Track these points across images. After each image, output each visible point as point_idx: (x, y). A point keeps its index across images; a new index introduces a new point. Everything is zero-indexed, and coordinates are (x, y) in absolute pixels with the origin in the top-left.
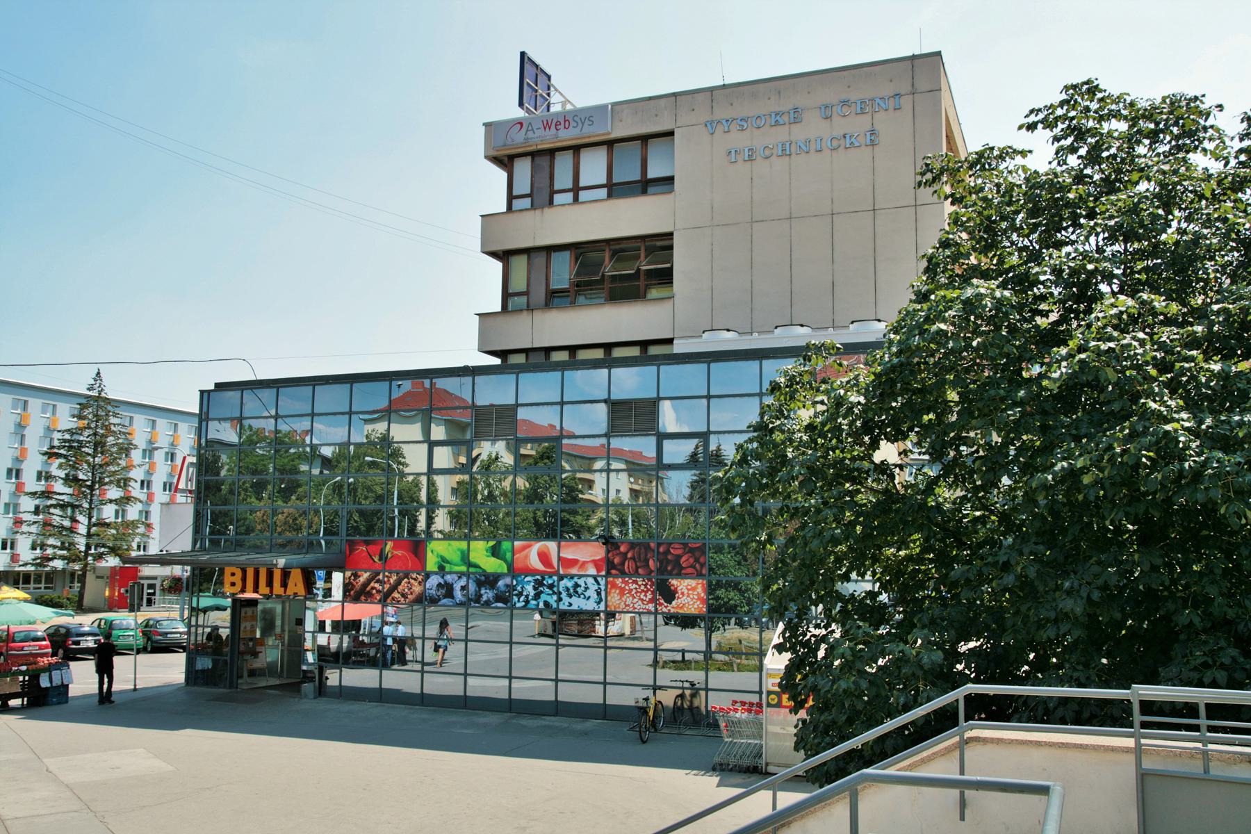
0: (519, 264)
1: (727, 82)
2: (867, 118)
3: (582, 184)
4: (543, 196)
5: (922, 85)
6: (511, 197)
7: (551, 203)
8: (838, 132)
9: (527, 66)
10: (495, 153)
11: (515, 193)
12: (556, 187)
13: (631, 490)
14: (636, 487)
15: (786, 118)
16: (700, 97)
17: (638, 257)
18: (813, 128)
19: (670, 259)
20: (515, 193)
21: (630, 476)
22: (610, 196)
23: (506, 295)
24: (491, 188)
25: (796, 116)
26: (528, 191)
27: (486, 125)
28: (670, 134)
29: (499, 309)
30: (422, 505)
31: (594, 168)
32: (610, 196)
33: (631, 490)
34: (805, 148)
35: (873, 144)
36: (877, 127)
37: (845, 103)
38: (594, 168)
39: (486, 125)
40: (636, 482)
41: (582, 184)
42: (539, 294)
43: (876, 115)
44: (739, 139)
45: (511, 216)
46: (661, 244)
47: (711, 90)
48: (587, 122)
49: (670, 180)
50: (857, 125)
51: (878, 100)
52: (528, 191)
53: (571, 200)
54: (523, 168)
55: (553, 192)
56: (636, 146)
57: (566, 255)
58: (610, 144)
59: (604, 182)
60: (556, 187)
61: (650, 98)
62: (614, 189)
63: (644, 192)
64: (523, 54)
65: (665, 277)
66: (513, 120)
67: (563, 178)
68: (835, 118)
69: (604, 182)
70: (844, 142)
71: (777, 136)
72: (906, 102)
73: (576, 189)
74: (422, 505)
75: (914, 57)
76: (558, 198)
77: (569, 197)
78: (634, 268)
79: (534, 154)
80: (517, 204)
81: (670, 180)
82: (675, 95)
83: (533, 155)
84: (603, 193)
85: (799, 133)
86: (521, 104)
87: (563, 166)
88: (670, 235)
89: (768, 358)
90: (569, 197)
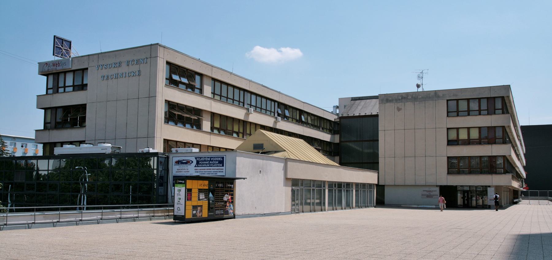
0: (49, 112)
3: (66, 85)
5: (153, 55)
6: (47, 89)
7: (58, 92)
8: (130, 71)
9: (56, 40)
16: (95, 56)
18: (124, 69)
22: (74, 90)
23: (45, 123)
24: (41, 84)
27: (38, 63)
28: (87, 69)
29: (43, 128)
30: (35, 170)
31: (69, 81)
32: (74, 90)
35: (139, 75)
37: (133, 61)
39: (38, 63)
41: (66, 85)
43: (142, 65)
44: (105, 72)
46: (83, 107)
47: (98, 54)
50: (135, 68)
52: (486, 109)
54: (51, 78)
55: (495, 109)
57: (61, 109)
58: (74, 71)
64: (55, 36)
65: (83, 119)
67: (61, 84)
70: (131, 75)
73: (65, 87)
74: (35, 170)
75: (151, 45)
76: (61, 90)
79: (54, 74)
82: (89, 55)
84: (71, 89)
85: (121, 70)
88: (86, 104)
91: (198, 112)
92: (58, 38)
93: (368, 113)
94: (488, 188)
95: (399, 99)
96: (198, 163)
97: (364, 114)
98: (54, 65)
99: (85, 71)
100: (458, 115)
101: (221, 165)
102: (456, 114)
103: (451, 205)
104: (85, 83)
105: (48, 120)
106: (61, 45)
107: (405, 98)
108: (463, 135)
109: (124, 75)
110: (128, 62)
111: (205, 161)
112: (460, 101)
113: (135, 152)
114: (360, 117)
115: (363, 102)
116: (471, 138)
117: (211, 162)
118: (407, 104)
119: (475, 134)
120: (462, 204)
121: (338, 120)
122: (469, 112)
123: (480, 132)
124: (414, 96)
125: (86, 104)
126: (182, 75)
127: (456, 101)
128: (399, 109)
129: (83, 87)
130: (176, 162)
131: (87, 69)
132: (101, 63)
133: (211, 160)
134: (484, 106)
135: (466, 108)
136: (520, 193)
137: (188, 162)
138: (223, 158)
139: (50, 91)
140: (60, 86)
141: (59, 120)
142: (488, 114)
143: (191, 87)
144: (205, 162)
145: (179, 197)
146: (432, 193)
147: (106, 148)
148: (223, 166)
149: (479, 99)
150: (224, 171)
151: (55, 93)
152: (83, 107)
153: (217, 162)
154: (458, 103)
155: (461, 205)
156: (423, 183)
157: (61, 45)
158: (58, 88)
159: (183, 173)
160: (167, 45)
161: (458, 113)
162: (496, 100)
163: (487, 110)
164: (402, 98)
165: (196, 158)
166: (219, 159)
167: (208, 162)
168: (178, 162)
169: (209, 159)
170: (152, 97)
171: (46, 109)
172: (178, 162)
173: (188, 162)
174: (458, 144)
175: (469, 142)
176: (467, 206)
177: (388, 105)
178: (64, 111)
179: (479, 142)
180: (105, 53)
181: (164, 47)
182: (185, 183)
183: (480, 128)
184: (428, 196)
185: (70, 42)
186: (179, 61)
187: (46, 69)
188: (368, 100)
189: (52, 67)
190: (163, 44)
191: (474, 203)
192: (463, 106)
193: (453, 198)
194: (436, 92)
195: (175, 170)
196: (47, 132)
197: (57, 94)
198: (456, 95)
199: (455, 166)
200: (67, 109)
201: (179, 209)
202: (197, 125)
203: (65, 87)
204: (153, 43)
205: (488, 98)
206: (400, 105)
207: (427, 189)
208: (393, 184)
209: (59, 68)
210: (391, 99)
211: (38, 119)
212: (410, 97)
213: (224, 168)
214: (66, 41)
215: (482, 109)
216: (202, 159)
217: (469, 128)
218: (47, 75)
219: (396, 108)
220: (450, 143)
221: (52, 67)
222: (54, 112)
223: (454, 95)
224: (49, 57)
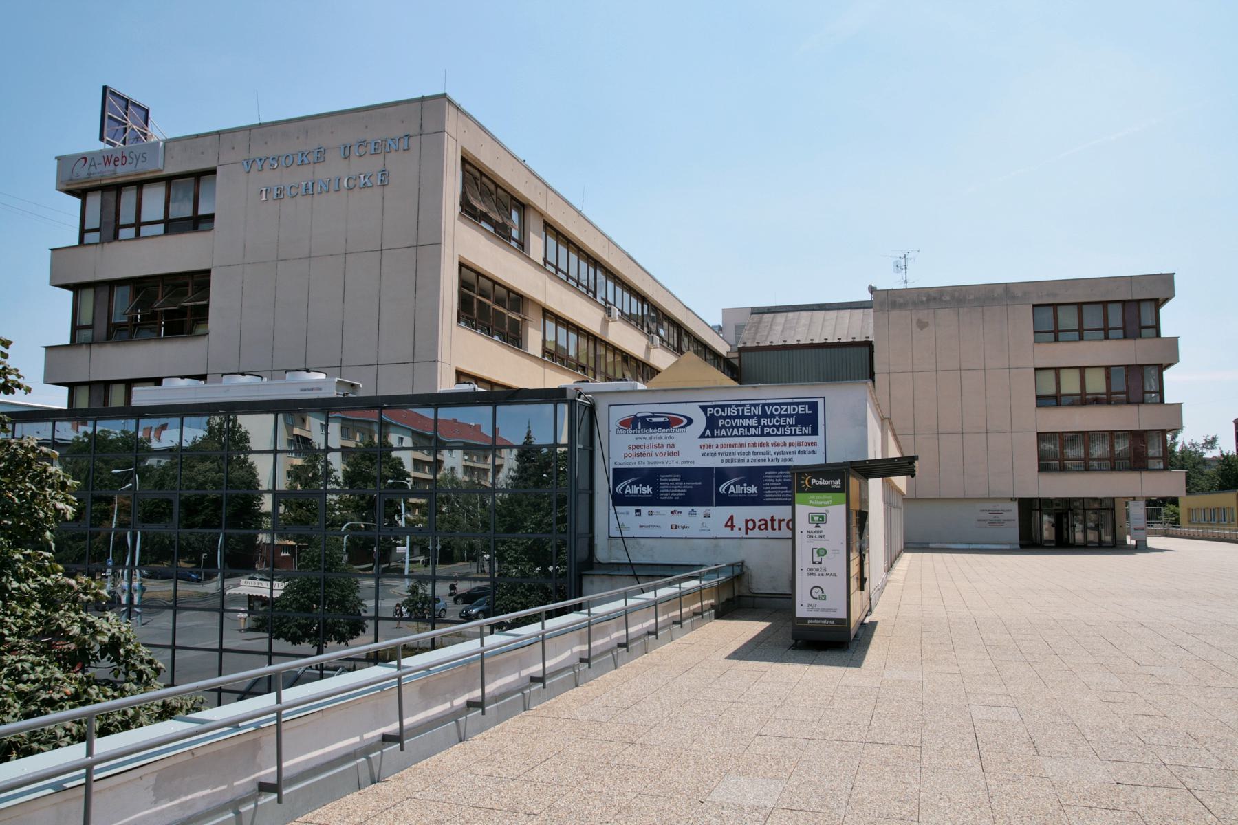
1: (263, 121)
2: (381, 157)
3: (143, 219)
4: (110, 230)
6: (83, 231)
7: (116, 237)
9: (110, 98)
10: (65, 187)
11: (87, 227)
12: (122, 222)
13: (465, 467)
14: (469, 464)
15: (311, 158)
17: (186, 294)
18: (334, 167)
19: (207, 297)
20: (87, 227)
21: (465, 454)
22: (166, 232)
23: (76, 328)
24: (63, 219)
25: (320, 155)
26: (97, 226)
27: (58, 158)
28: (212, 172)
29: (68, 342)
32: (166, 232)
33: (465, 467)
34: (327, 187)
35: (383, 184)
36: (388, 168)
37: (362, 143)
38: (154, 203)
39: (58, 158)
40: (471, 460)
41: (143, 219)
42: (102, 329)
43: (388, 156)
45: (82, 249)
46: (200, 281)
47: (250, 128)
48: (141, 159)
49: (210, 218)
50: (373, 164)
51: (389, 141)
53: (133, 236)
54: (95, 201)
56: (188, 186)
58: (168, 180)
59: (162, 217)
60: (122, 222)
61: (198, 136)
62: (172, 225)
63: (195, 228)
64: (105, 88)
65: (201, 314)
66: (78, 155)
67: (127, 216)
68: (354, 159)
69: (162, 217)
71: (301, 176)
72: (414, 142)
73: (138, 224)
75: (423, 99)
76: (123, 233)
77: (131, 232)
78: (172, 306)
79: (103, 191)
80: (89, 238)
81: (210, 218)
82: (218, 133)
83: (103, 189)
84: (160, 229)
85: (322, 173)
86: (102, 138)
87: (128, 198)
88: (209, 271)
89: (144, 417)
90: (131, 232)
91: (517, 300)
92: (113, 93)
93: (791, 341)
94: (1131, 503)
95: (922, 302)
96: (712, 423)
97: (768, 344)
98: (107, 161)
99: (205, 183)
100: (1057, 340)
101: (808, 430)
102: (1101, 333)
103: (1029, 542)
104: (201, 212)
105: (86, 318)
106: (119, 112)
107: (935, 299)
108: (1070, 385)
109: (333, 186)
110: (347, 148)
111: (743, 417)
112: (1059, 308)
113: (409, 392)
114: (785, 347)
115: (780, 318)
116: (1063, 391)
117: (764, 421)
118: (942, 313)
119: (1096, 384)
120: (1053, 538)
121: (736, 355)
122: (1081, 334)
123: (1108, 378)
124: (957, 294)
125: (209, 271)
126: (494, 201)
127: (1051, 309)
128: (922, 325)
129: (199, 222)
130: (624, 423)
131: (212, 172)
132: (256, 153)
133: (764, 415)
134: (1116, 318)
135: (1074, 324)
136: (1138, 511)
137: (670, 423)
138: (814, 406)
139: (94, 237)
140: (122, 222)
141: (116, 319)
142: (1125, 337)
143: (501, 233)
144: (740, 422)
145: (819, 544)
146: (1001, 517)
147: (318, 386)
148: (815, 432)
149: (1105, 304)
150: (820, 448)
151: (109, 242)
152: (200, 281)
153: (792, 421)
154: (1062, 311)
155: (1051, 541)
156: (982, 492)
157: (119, 112)
158: (118, 227)
159: (652, 459)
160: (464, 107)
161: (1056, 335)
162: (1143, 306)
163: (1124, 328)
164: (928, 300)
165: (704, 408)
166: (800, 410)
167: (754, 422)
168: (636, 423)
169: (758, 411)
170: (426, 245)
171: (76, 288)
172: (636, 423)
173: (670, 423)
174: (1058, 405)
175: (1085, 400)
176: (1063, 544)
177: (895, 314)
178: (136, 292)
179: (1105, 400)
180: (273, 124)
181: (458, 108)
182: (844, 489)
183: (1107, 368)
184: (992, 523)
185: (147, 111)
186: (487, 158)
187: (82, 172)
188: (791, 315)
189: (101, 168)
190: (457, 100)
191: (1079, 537)
192: (1068, 319)
193: (1050, 527)
194: (1007, 287)
195: (620, 449)
196: (83, 352)
197: (116, 244)
198: (1056, 295)
199: (1054, 453)
200: (142, 286)
201: (818, 593)
202: (514, 338)
203: (138, 224)
204: (426, 95)
205: (1123, 302)
206: (924, 314)
207: (990, 506)
208: (961, 496)
209: (124, 171)
210: (902, 300)
211: (54, 317)
212: (948, 298)
213: (819, 439)
214: (134, 104)
215: (1085, 327)
216: (727, 412)
217: (1082, 369)
218: (81, 193)
219: (914, 322)
220: (1043, 401)
221: (101, 168)
222: (104, 294)
223: (1048, 295)
224: (90, 143)
